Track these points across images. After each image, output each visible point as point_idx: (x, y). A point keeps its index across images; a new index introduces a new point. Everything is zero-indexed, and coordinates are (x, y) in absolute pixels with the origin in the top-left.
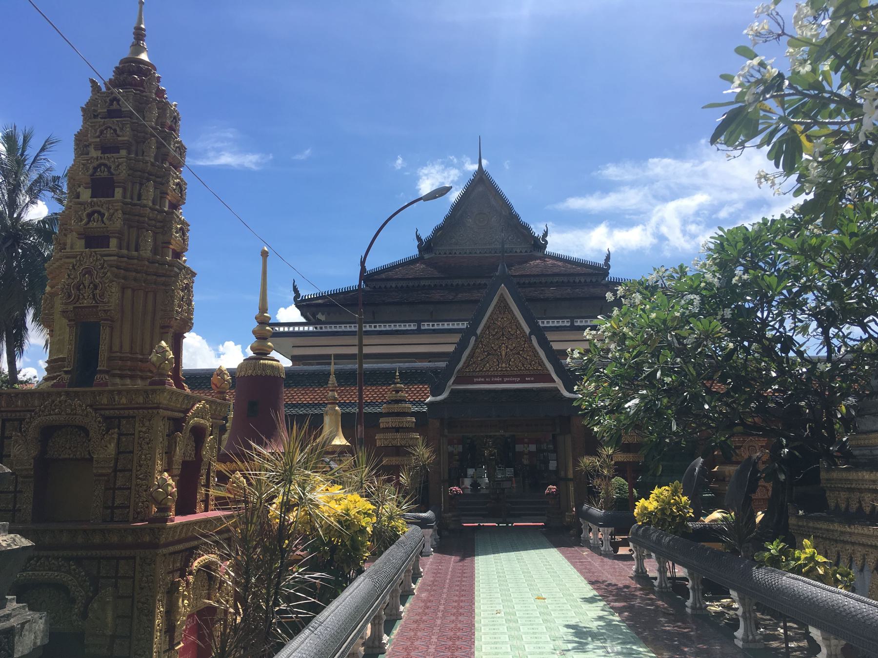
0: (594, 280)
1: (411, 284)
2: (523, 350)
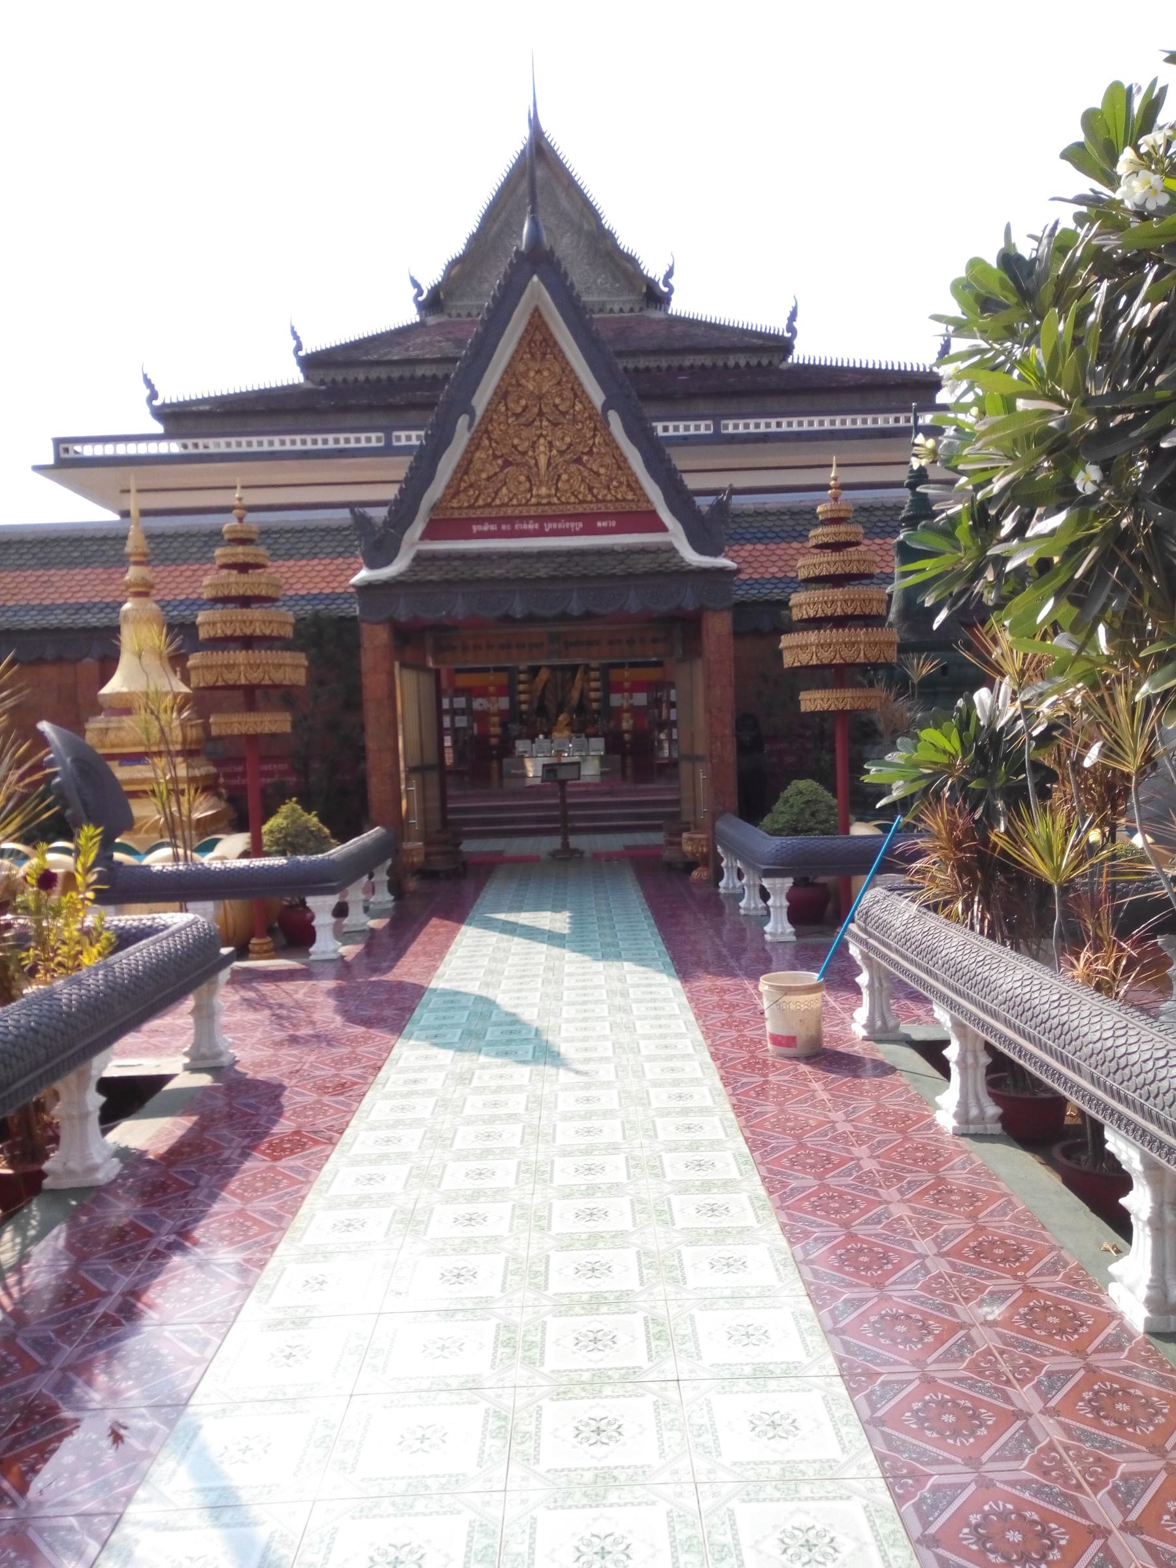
0: (765, 362)
1: (396, 373)
2: (590, 453)
